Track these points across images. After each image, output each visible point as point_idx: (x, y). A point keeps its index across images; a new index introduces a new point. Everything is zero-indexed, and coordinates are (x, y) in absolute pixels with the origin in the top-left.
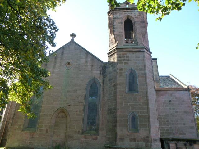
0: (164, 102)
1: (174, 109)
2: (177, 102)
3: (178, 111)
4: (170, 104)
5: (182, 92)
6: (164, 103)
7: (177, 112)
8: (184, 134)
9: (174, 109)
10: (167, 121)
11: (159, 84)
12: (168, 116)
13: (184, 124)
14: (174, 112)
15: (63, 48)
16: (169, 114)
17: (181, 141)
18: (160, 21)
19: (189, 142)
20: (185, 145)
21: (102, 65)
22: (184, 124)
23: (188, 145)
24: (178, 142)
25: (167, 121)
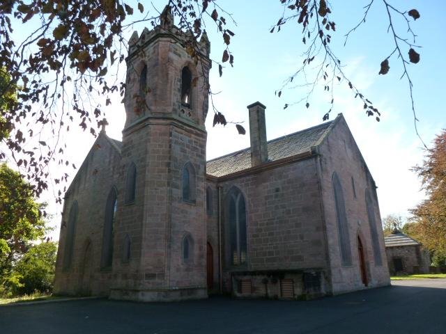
0: (266, 194)
1: (283, 207)
2: (292, 190)
3: (291, 209)
4: (276, 196)
5: (301, 164)
6: (267, 198)
7: (288, 212)
8: (300, 258)
9: (283, 207)
10: (271, 234)
11: (259, 157)
12: (273, 224)
13: (302, 238)
14: (283, 213)
15: (203, 134)
16: (274, 219)
17: (258, 275)
18: (334, 30)
19: (271, 276)
20: (265, 282)
21: (249, 152)
22: (302, 238)
23: (270, 281)
24: (254, 277)
25: (271, 234)
